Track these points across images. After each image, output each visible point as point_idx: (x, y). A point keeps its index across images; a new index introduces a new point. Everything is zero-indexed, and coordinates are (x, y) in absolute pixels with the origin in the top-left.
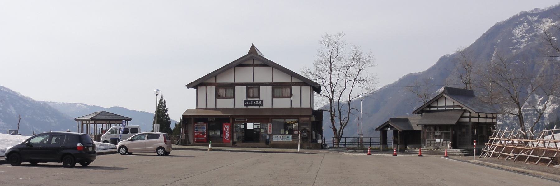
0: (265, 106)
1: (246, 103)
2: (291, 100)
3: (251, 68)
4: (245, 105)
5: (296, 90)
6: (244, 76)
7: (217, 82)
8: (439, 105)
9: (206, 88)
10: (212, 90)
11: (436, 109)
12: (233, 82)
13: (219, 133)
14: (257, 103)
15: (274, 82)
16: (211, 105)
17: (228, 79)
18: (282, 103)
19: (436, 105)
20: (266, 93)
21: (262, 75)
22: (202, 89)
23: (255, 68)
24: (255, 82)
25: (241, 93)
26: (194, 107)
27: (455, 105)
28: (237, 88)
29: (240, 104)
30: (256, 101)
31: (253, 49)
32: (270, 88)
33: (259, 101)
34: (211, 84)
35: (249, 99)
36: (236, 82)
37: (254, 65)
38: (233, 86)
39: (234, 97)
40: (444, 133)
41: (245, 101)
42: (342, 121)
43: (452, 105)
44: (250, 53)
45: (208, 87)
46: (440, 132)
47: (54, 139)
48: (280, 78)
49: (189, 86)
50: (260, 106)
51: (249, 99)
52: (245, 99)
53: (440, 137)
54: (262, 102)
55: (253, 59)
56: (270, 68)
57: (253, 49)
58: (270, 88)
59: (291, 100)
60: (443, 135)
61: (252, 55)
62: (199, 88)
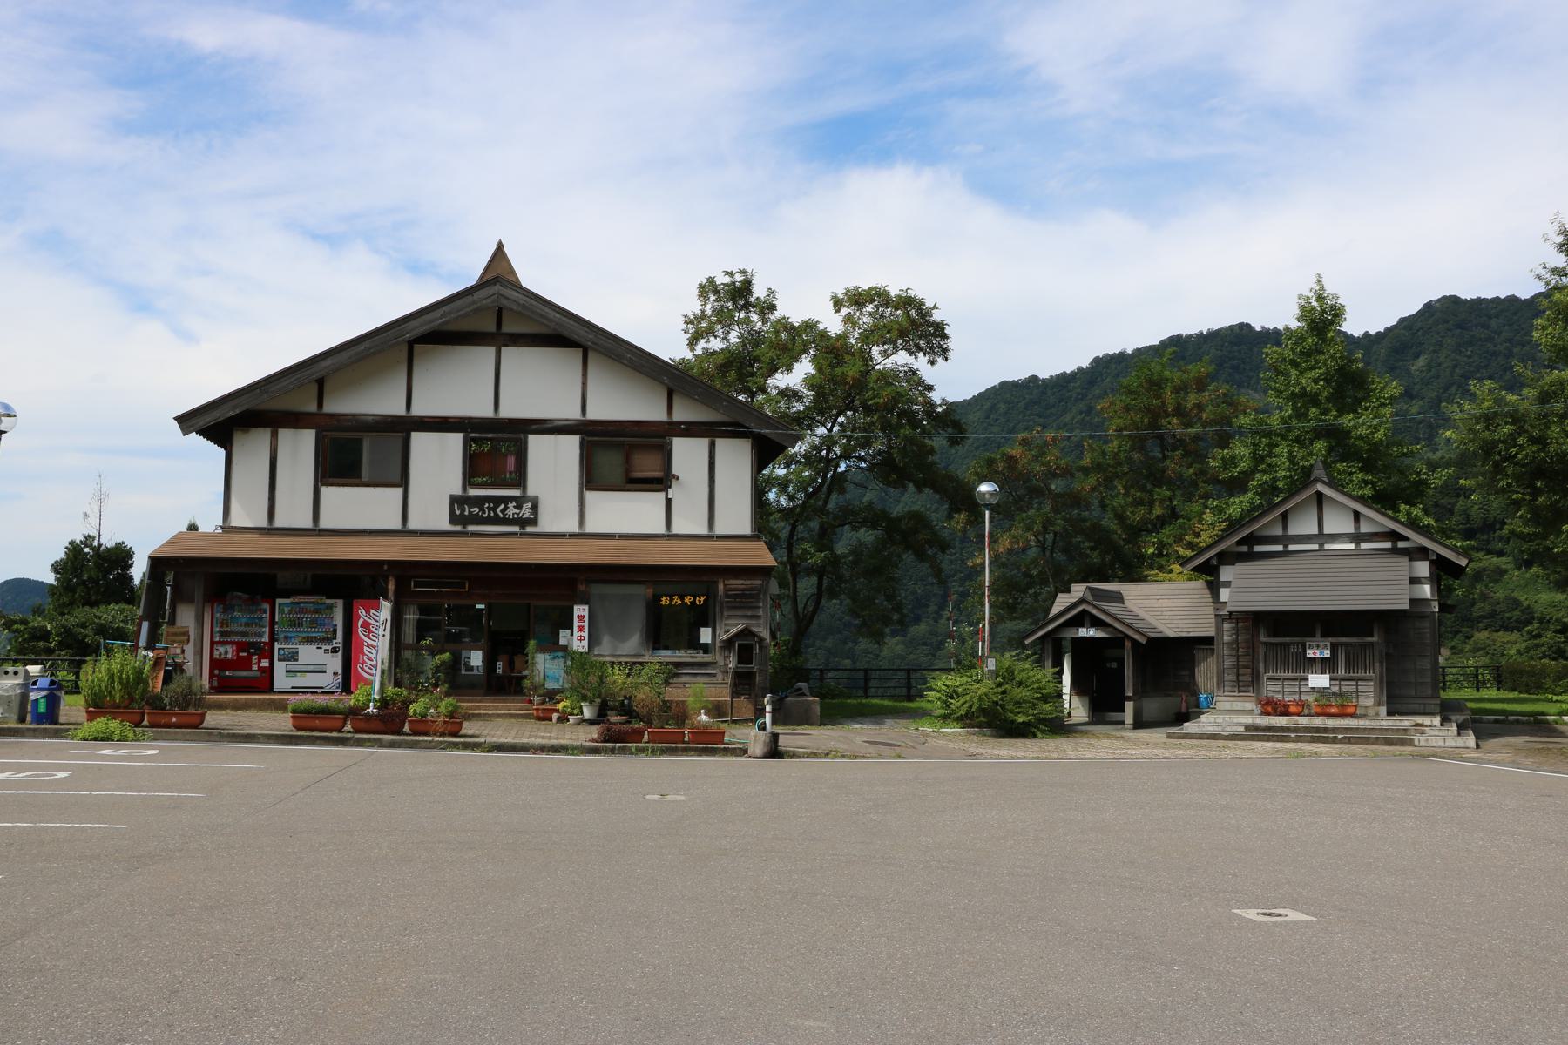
0: (547, 524)
1: (463, 511)
2: (669, 502)
3: (484, 356)
4: (454, 519)
5: (687, 455)
6: (459, 386)
7: (329, 407)
8: (1292, 531)
9: (274, 436)
10: (299, 449)
11: (1280, 548)
12: (401, 411)
13: (664, 601)
14: (512, 510)
15: (592, 415)
16: (294, 512)
17: (381, 400)
18: (626, 515)
19: (1278, 531)
20: (553, 467)
21: (537, 386)
22: (253, 448)
23: (508, 353)
24: (505, 413)
25: (438, 465)
26: (210, 522)
27: (1365, 528)
28: (419, 440)
29: (430, 510)
30: (506, 500)
31: (499, 270)
32: (571, 444)
33: (519, 501)
34: (296, 420)
35: (473, 492)
36: (419, 409)
37: (499, 338)
38: (403, 427)
39: (403, 481)
40: (1347, 645)
41: (454, 500)
42: (800, 607)
43: (1349, 528)
44: (486, 281)
45: (285, 435)
46: (1328, 641)
47: (1114, 665)
48: (619, 402)
49: (187, 421)
50: (523, 522)
51: (473, 492)
52: (457, 490)
53: (1326, 665)
54: (535, 508)
55: (498, 314)
56: (572, 357)
57: (499, 270)
58: (571, 444)
59: (669, 502)
60: (1341, 658)
61: (497, 288)
62: (241, 442)
